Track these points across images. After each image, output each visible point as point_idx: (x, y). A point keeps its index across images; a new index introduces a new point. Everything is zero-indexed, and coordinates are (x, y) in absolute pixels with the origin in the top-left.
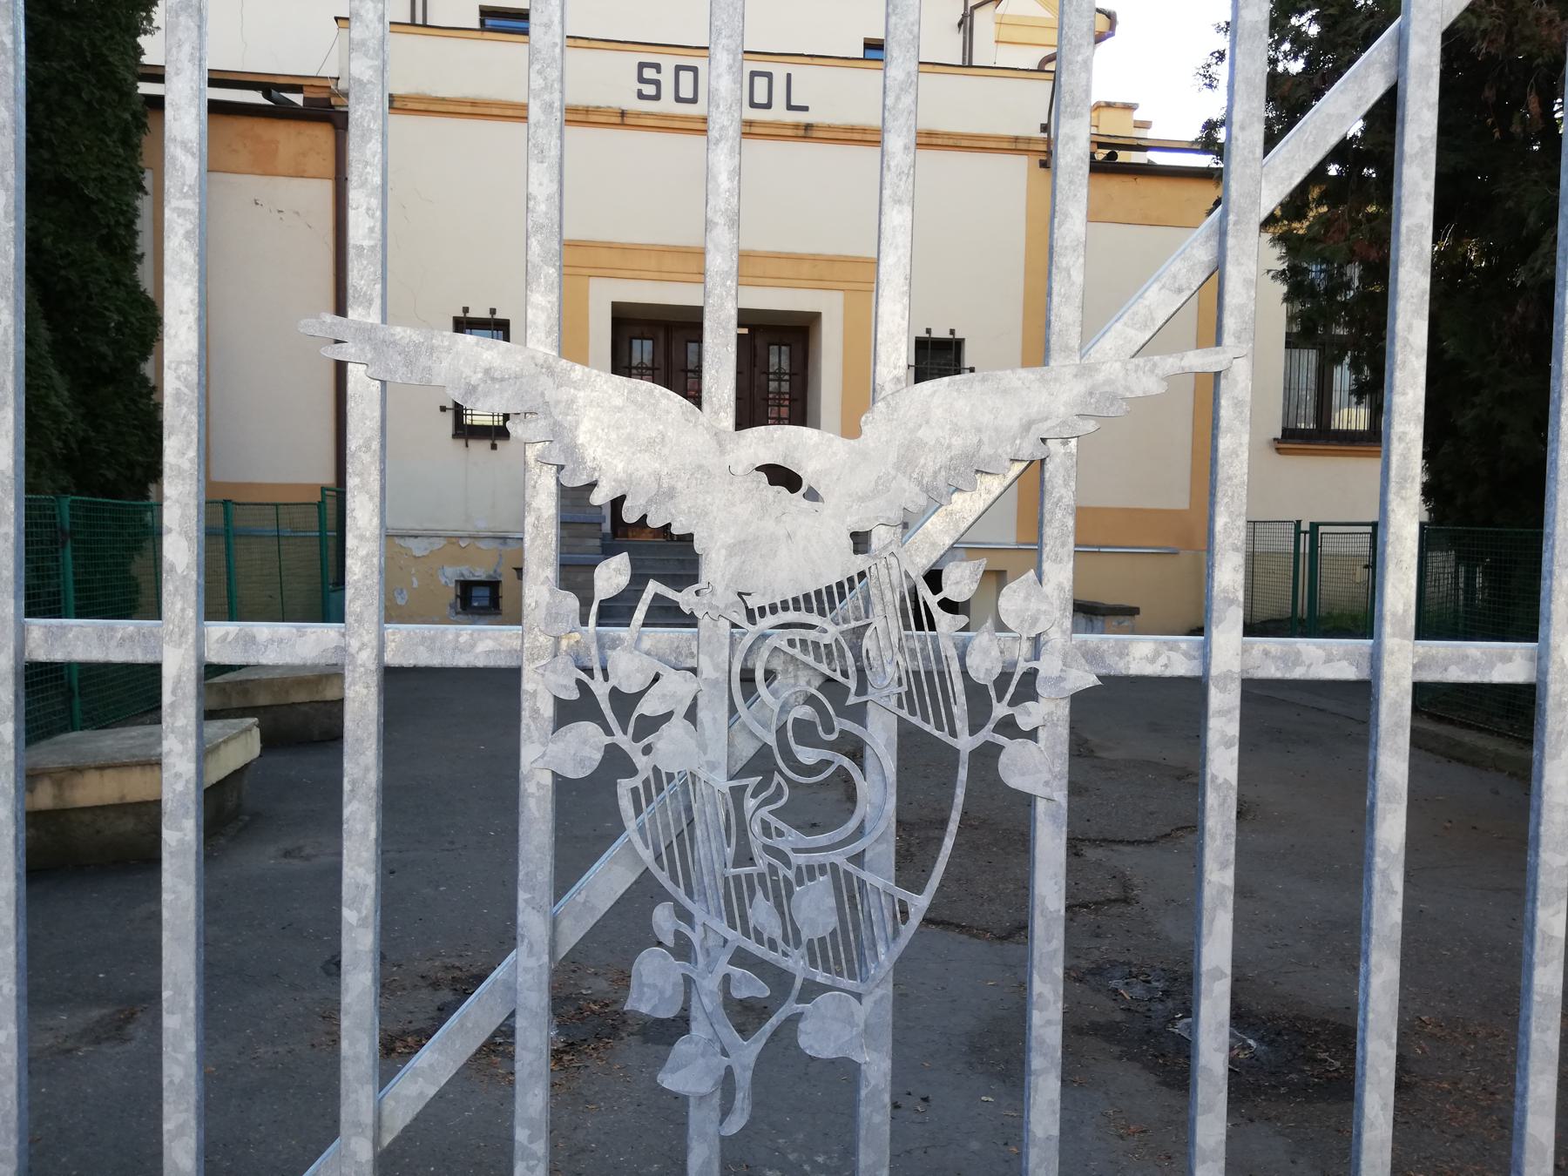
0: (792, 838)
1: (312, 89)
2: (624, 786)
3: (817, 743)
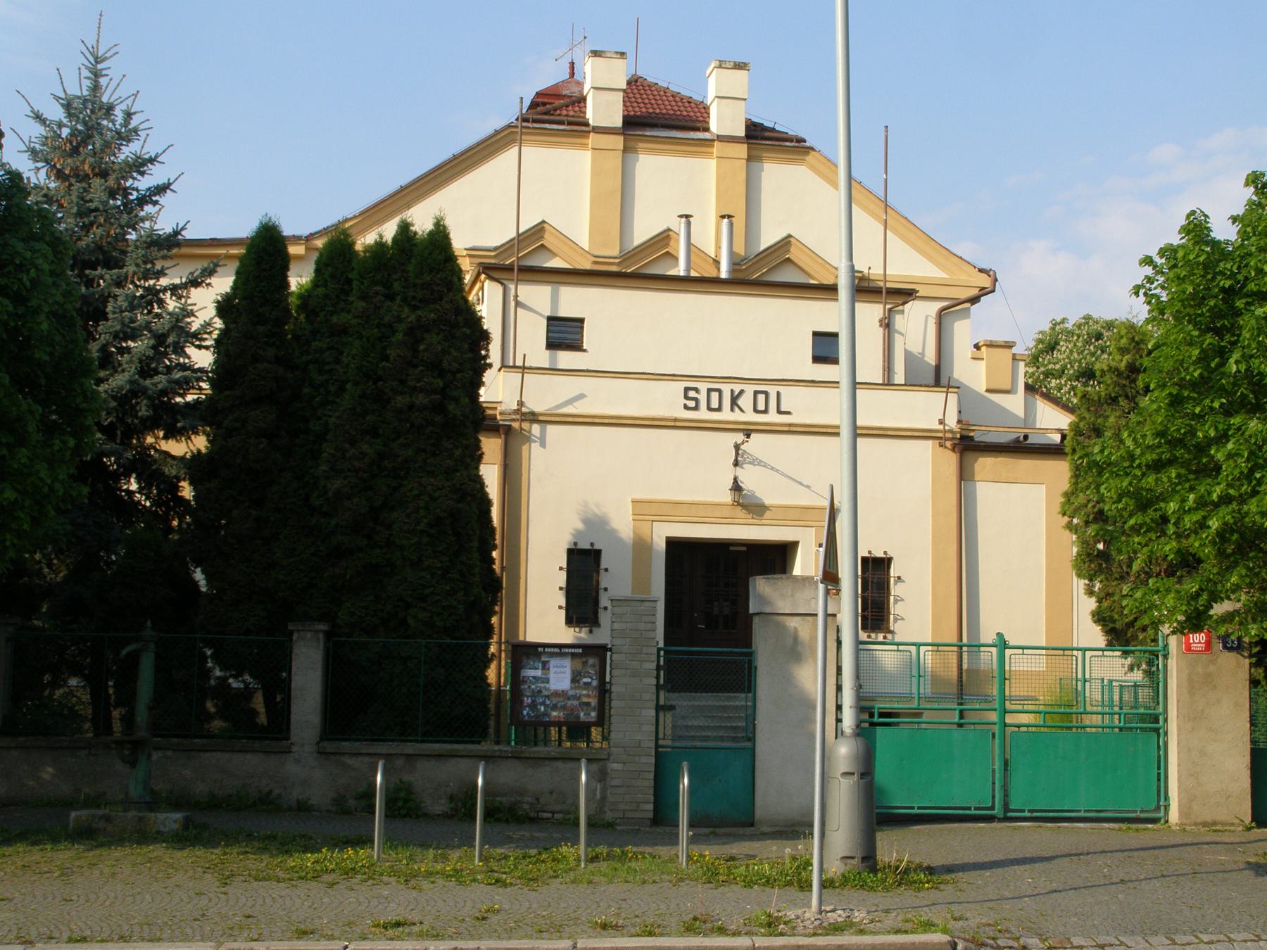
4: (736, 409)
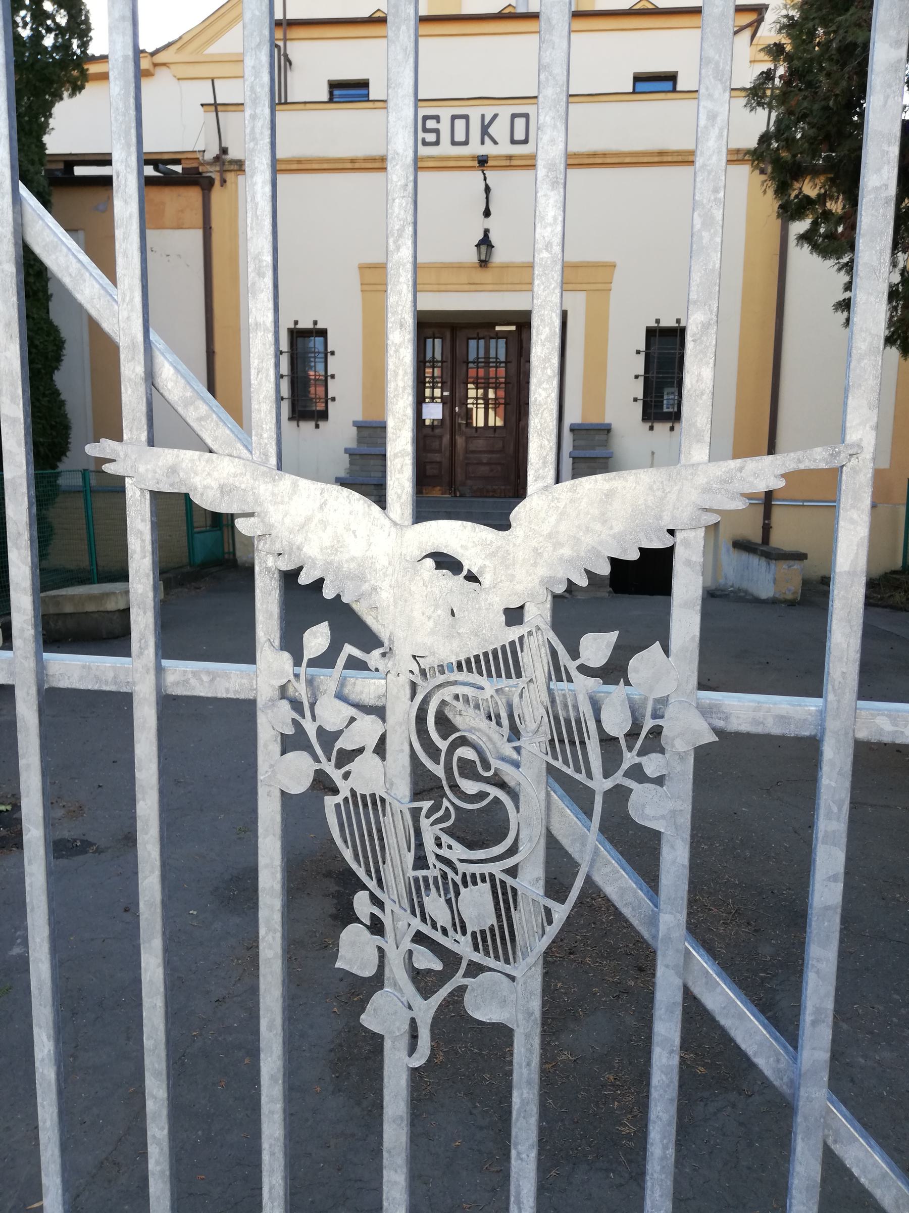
0: (458, 852)
1: (187, 162)
2: (330, 801)
3: (478, 778)
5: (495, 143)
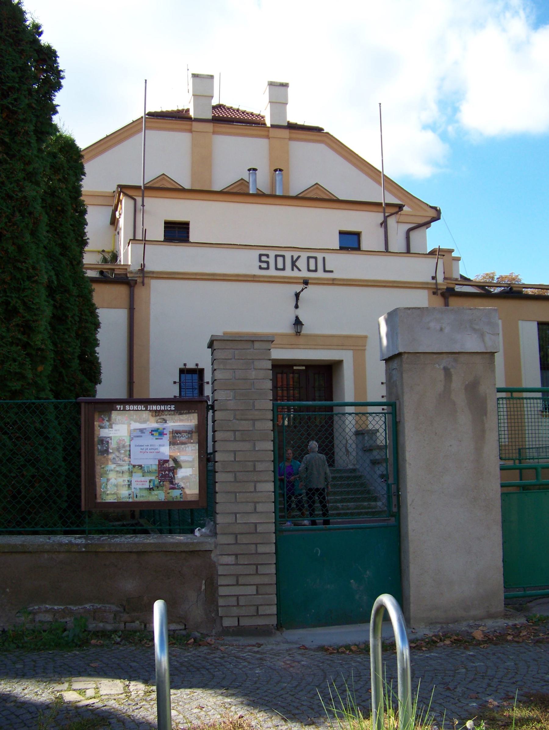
4: (295, 268)
5: (299, 270)
